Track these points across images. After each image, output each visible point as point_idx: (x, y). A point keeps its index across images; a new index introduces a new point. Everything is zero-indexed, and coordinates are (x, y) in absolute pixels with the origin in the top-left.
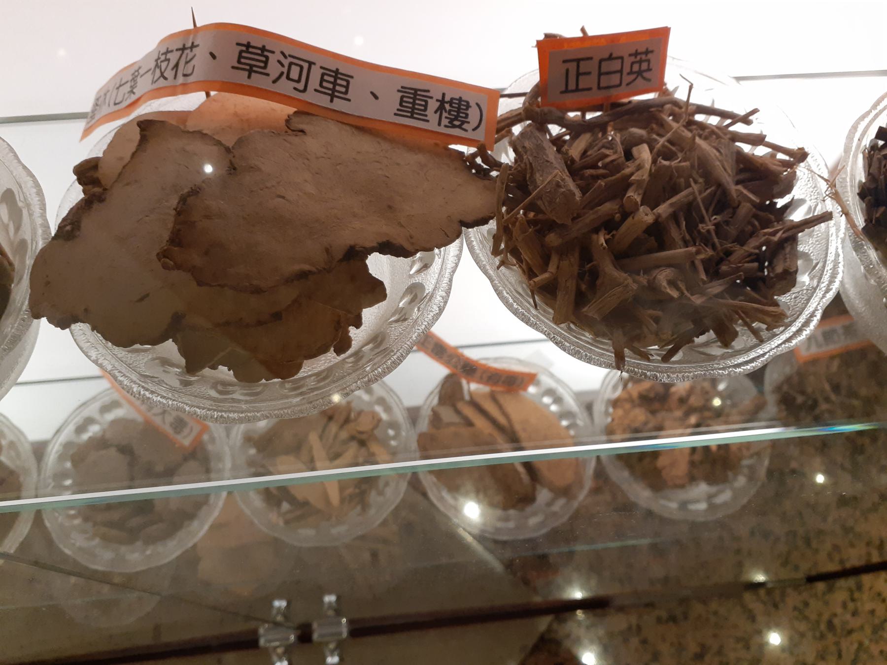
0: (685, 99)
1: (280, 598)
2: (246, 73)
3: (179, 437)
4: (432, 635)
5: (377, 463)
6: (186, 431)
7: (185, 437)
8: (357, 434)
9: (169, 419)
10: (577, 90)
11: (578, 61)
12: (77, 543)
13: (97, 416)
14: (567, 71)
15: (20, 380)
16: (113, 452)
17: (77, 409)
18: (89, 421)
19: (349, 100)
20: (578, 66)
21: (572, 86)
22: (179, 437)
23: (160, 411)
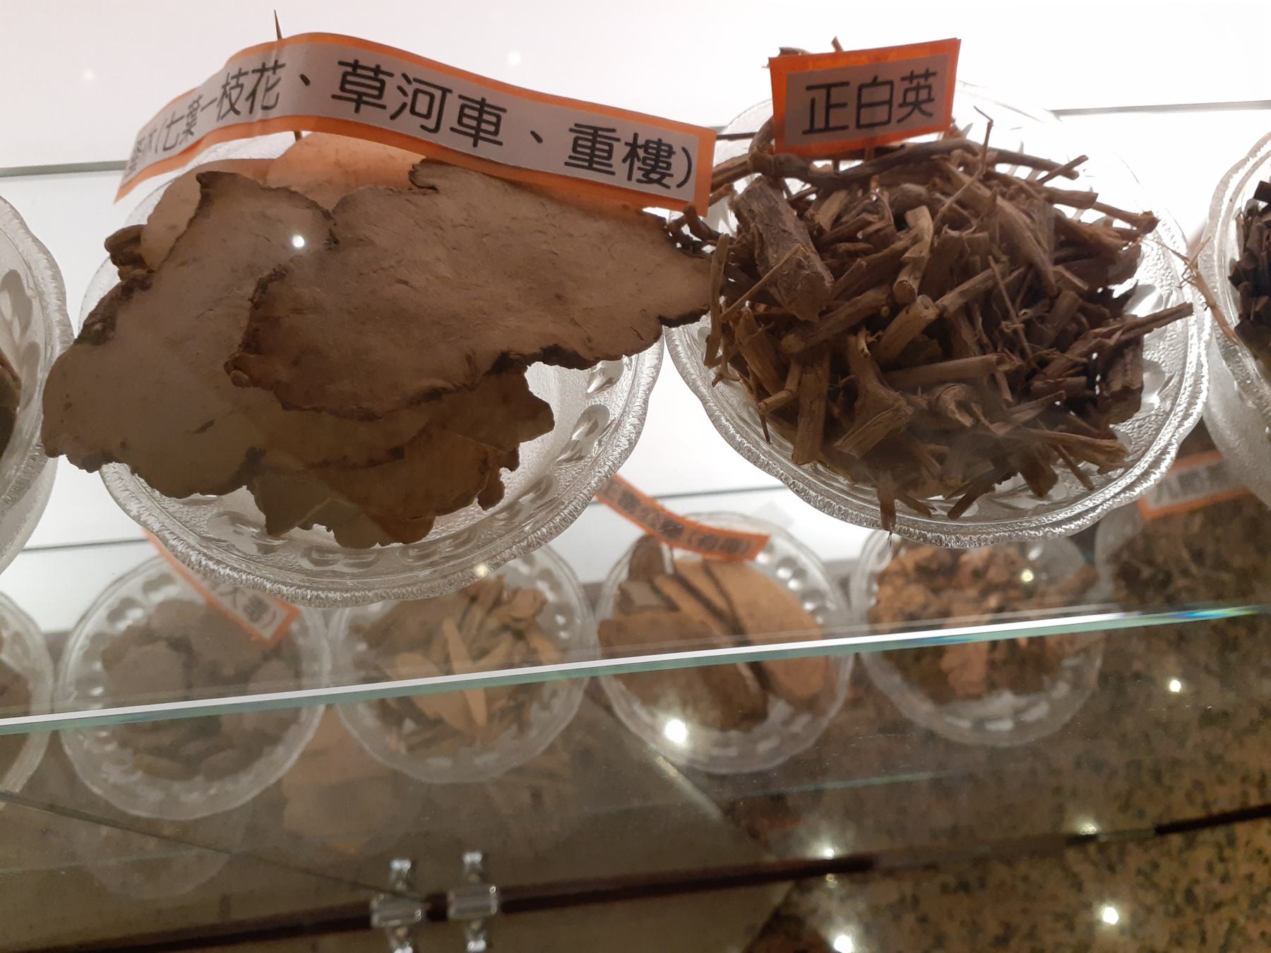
0: (981, 141)
1: (402, 857)
2: (353, 105)
3: (256, 627)
4: (620, 910)
5: (540, 664)
6: (267, 617)
7: (265, 627)
8: (511, 621)
9: (242, 600)
10: (827, 128)
11: (829, 87)
12: (111, 778)
13: (139, 596)
14: (813, 102)
15: (28, 544)
16: (161, 647)
17: (111, 586)
18: (128, 603)
19: (500, 144)
20: (828, 95)
21: (820, 123)
22: (256, 627)
23: (230, 589)
